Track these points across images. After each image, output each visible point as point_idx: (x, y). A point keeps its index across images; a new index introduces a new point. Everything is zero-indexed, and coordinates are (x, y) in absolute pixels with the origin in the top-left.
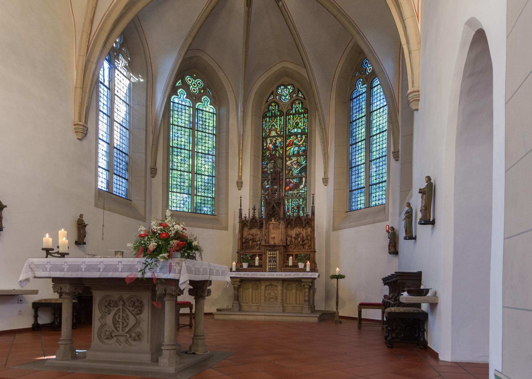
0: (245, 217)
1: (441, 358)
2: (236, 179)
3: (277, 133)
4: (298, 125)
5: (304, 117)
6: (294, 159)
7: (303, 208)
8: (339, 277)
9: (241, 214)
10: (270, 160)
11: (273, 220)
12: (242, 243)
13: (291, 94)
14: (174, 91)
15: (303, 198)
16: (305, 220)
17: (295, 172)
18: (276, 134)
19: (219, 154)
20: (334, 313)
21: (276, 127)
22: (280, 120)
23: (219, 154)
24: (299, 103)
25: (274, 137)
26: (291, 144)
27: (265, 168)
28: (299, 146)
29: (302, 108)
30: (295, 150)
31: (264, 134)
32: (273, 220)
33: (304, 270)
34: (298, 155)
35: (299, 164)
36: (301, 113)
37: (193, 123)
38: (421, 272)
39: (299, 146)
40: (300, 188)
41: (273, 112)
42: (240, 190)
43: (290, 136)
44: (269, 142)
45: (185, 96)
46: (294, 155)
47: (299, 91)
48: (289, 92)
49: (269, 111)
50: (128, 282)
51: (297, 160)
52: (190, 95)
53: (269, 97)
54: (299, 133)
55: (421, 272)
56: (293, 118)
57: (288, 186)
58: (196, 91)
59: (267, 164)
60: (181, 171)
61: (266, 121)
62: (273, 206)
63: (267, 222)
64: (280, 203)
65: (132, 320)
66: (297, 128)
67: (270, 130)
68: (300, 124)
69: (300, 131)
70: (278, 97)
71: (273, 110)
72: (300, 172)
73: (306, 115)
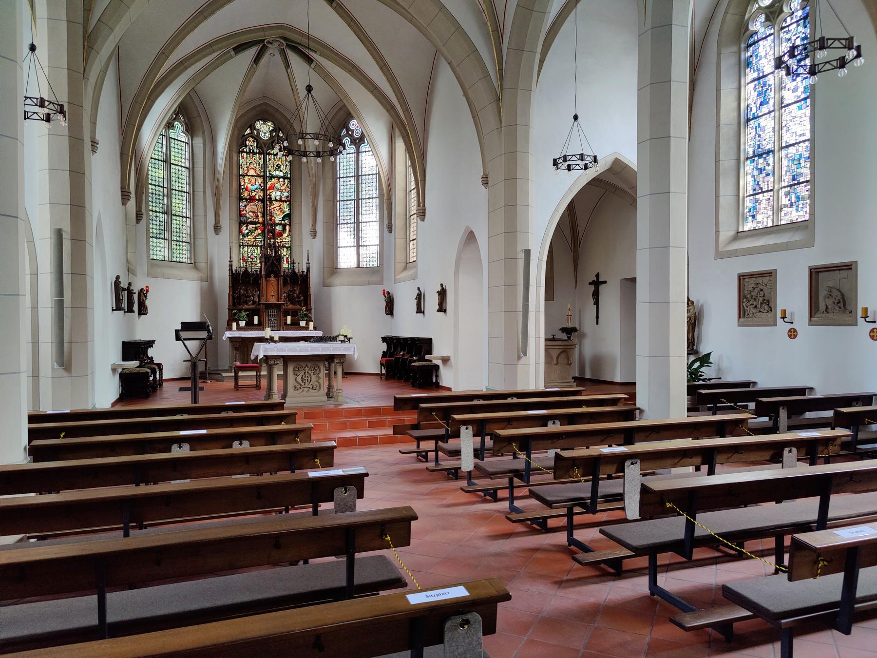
6: (276, 204)
15: (287, 248)
17: (278, 218)
19: (193, 191)
26: (272, 187)
28: (281, 191)
33: (306, 328)
34: (281, 200)
38: (431, 339)
44: (247, 181)
46: (276, 200)
47: (280, 130)
50: (860, 403)
54: (281, 177)
55: (431, 339)
59: (245, 206)
60: (156, 212)
61: (243, 157)
64: (279, 258)
65: (314, 378)
69: (281, 174)
72: (283, 219)
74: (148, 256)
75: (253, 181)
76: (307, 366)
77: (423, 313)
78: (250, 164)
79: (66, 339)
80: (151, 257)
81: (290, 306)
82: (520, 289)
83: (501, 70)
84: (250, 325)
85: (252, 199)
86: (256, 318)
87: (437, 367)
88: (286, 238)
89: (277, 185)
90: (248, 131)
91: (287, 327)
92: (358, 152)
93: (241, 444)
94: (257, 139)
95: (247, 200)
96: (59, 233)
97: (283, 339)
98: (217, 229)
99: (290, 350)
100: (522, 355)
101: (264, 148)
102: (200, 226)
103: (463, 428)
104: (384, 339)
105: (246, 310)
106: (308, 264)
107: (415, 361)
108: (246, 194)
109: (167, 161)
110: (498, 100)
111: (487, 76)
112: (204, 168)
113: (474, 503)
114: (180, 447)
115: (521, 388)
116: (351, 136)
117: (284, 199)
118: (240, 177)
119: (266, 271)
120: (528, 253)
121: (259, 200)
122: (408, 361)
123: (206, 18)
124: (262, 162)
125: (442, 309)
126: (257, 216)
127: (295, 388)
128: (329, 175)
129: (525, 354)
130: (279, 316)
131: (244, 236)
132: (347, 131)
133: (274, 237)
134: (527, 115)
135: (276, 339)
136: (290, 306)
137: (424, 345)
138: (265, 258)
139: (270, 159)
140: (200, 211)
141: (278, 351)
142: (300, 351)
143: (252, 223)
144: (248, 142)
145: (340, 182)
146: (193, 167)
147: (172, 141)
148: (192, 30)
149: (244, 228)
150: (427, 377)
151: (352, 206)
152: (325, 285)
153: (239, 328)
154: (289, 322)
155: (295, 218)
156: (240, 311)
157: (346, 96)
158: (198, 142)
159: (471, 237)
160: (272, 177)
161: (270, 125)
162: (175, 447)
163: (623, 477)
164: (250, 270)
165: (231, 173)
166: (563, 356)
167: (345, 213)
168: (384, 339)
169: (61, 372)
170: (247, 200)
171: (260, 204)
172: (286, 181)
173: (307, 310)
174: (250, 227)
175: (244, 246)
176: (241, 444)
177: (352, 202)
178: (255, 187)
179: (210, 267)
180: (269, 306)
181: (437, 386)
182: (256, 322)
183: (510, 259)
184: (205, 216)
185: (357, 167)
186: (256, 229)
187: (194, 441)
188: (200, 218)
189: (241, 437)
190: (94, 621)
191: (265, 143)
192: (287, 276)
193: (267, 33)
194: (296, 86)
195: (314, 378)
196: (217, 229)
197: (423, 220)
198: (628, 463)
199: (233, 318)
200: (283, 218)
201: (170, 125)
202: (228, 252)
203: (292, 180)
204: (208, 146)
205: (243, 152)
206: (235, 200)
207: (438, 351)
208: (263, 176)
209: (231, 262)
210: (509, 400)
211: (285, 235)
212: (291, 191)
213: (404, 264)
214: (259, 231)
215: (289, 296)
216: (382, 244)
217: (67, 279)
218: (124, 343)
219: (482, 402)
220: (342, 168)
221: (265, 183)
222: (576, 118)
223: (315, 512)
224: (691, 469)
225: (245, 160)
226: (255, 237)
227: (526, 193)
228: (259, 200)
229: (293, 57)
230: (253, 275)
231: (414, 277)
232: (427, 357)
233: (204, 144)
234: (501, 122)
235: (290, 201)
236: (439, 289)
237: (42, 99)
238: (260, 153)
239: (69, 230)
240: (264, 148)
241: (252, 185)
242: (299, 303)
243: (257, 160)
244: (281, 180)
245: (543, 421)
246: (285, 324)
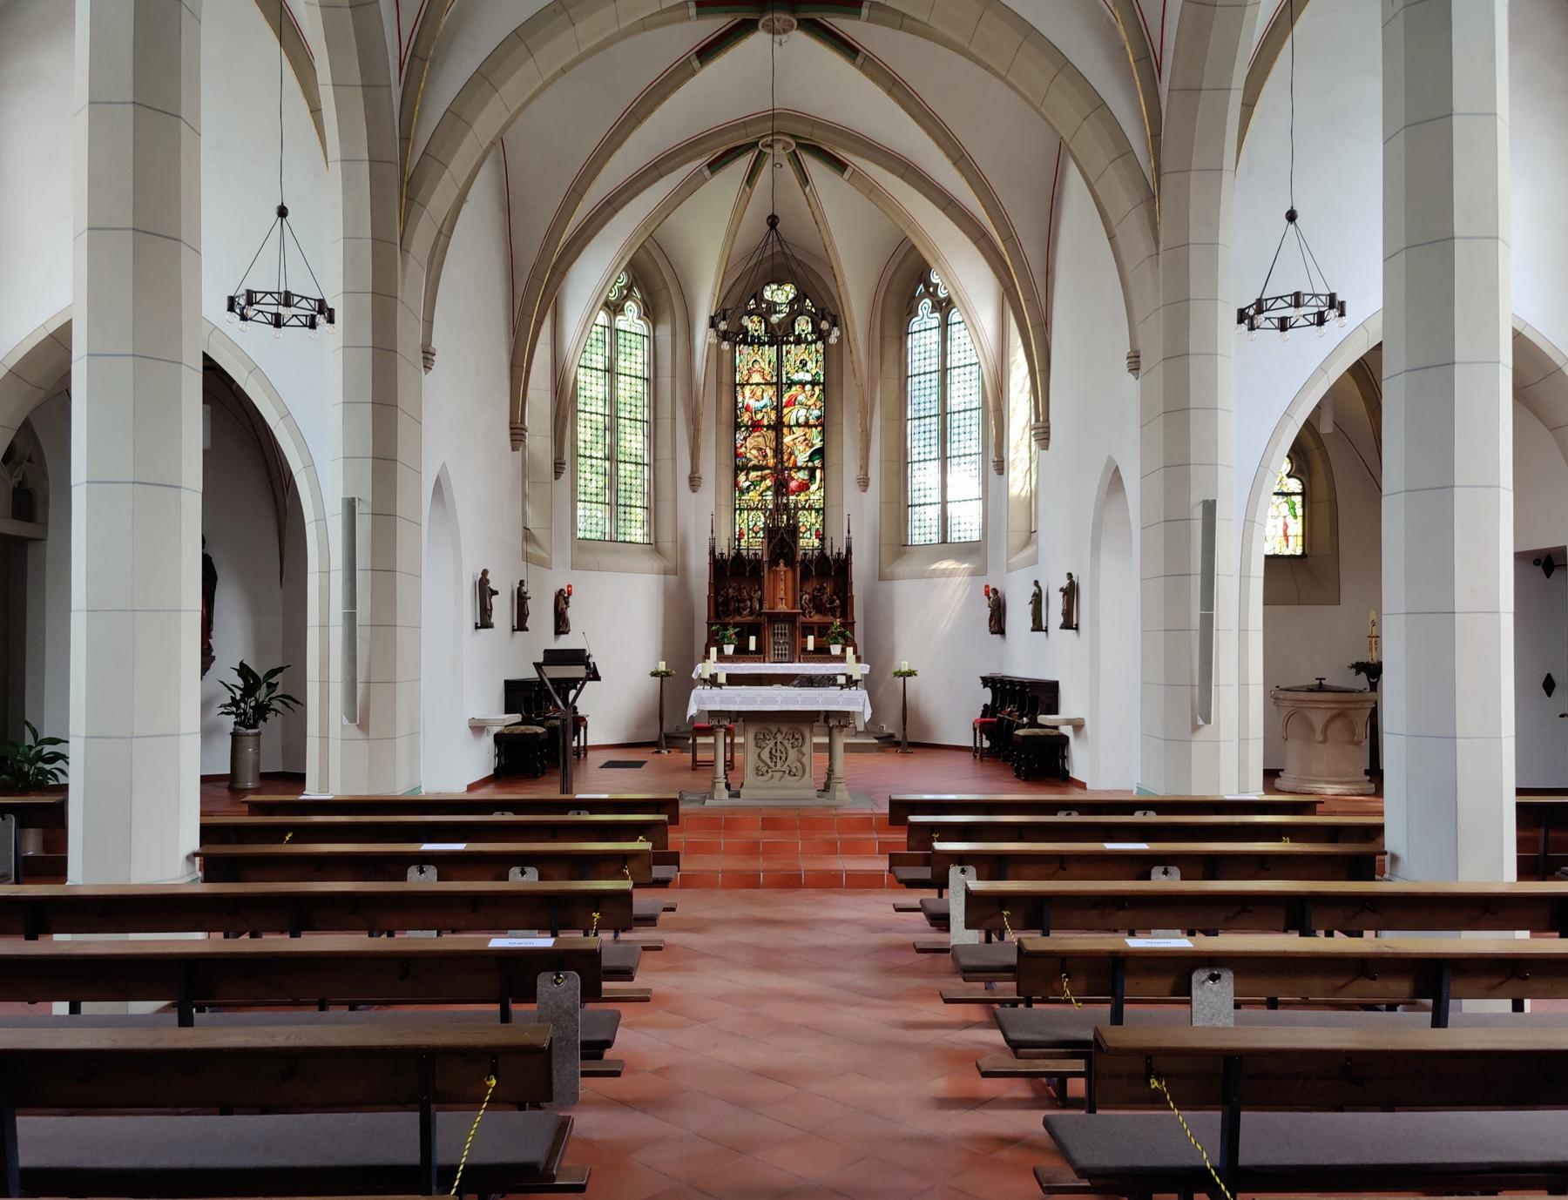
1: (1080, 763)
2: (687, 471)
6: (799, 432)
8: (911, 673)
9: (712, 552)
12: (717, 604)
15: (817, 511)
17: (802, 458)
20: (499, 738)
26: (792, 403)
28: (808, 408)
33: (842, 658)
34: (807, 425)
43: (790, 387)
46: (798, 425)
47: (806, 297)
63: (770, 567)
64: (793, 531)
65: (792, 753)
69: (808, 377)
72: (811, 458)
74: (574, 534)
75: (759, 393)
76: (779, 731)
77: (1077, 628)
78: (755, 362)
79: (361, 676)
80: (580, 535)
81: (816, 618)
82: (1196, 583)
83: (1156, 135)
84: (742, 652)
85: (756, 426)
86: (753, 639)
87: (1064, 740)
88: (815, 494)
89: (801, 398)
91: (806, 656)
92: (944, 325)
93: (523, 873)
95: (747, 427)
96: (350, 505)
97: (733, 680)
98: (694, 482)
99: (744, 701)
100: (1201, 722)
103: (954, 871)
104: (987, 681)
105: (735, 625)
107: (1024, 726)
108: (746, 417)
109: (611, 371)
110: (1151, 198)
111: (1125, 151)
112: (674, 377)
113: (968, 1025)
114: (422, 872)
115: (1199, 790)
116: (933, 296)
117: (812, 422)
119: (771, 554)
120: (1210, 508)
121: (769, 427)
122: (1021, 725)
123: (640, 122)
125: (1069, 624)
126: (765, 456)
127: (758, 772)
128: (891, 369)
129: (1207, 720)
130: (792, 635)
131: (742, 492)
132: (927, 287)
133: (787, 495)
134: (1212, 222)
135: (722, 679)
136: (816, 618)
137: (1044, 695)
138: (771, 532)
140: (665, 453)
141: (722, 702)
142: (762, 703)
143: (755, 468)
145: (913, 384)
146: (656, 377)
147: (621, 334)
148: (620, 144)
149: (742, 477)
150: (1045, 759)
151: (934, 427)
152: (882, 577)
153: (722, 658)
154: (811, 646)
156: (725, 627)
157: (911, 223)
158: (664, 331)
159: (1115, 481)
160: (791, 384)
161: (789, 291)
162: (413, 872)
163: (1189, 1003)
164: (744, 553)
165: (719, 383)
166: (1338, 724)
167: (921, 441)
168: (987, 681)
169: (353, 731)
170: (747, 427)
171: (771, 434)
172: (817, 389)
173: (842, 625)
174: (753, 474)
176: (523, 873)
177: (934, 420)
178: (762, 403)
179: (682, 547)
180: (775, 618)
181: (1062, 777)
182: (752, 646)
183: (1174, 520)
184: (674, 459)
185: (944, 354)
186: (763, 478)
187: (447, 865)
188: (665, 464)
189: (524, 860)
190: (413, 1157)
192: (811, 561)
193: (816, 131)
194: (822, 214)
195: (792, 753)
196: (694, 482)
197: (1046, 448)
198: (1199, 976)
199: (715, 640)
201: (614, 308)
202: (721, 520)
203: (827, 387)
204: (681, 339)
206: (726, 430)
207: (1071, 705)
210: (1138, 817)
211: (814, 487)
213: (1024, 535)
214: (768, 482)
215: (813, 599)
216: (985, 498)
217: (363, 579)
218: (507, 683)
219: (1075, 818)
220: (916, 357)
221: (780, 395)
222: (1291, 216)
223: (505, 1017)
224: (1505, 1005)
225: (745, 355)
226: (760, 493)
227: (1212, 384)
228: (769, 427)
229: (813, 165)
230: (750, 561)
231: (1034, 561)
232: (1043, 719)
233: (674, 335)
234: (1157, 242)
235: (822, 425)
236: (1065, 583)
237: (287, 293)
239: (369, 498)
241: (756, 400)
242: (833, 612)
244: (808, 387)
245: (1141, 866)
246: (804, 650)
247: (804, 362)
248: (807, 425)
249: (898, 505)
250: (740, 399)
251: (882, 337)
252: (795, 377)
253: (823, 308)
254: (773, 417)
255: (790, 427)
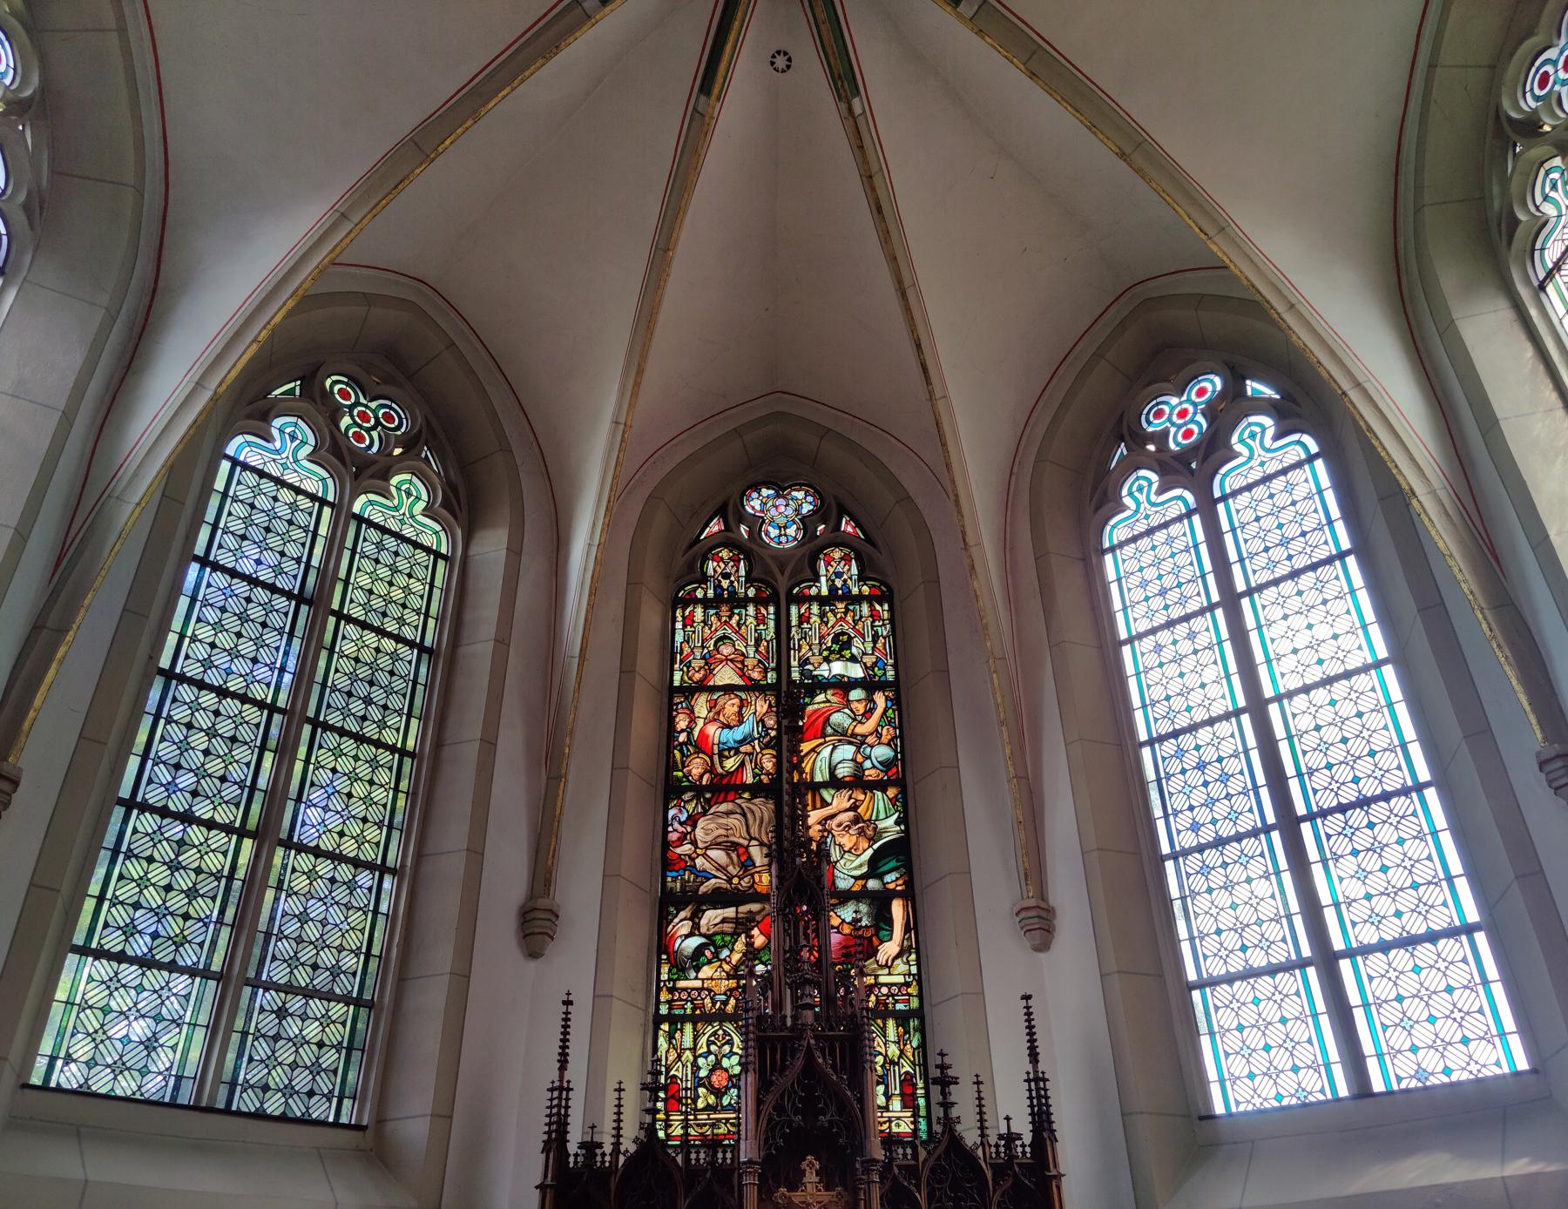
0: (590, 1147)
3: (742, 675)
4: (848, 645)
5: (874, 615)
7: (907, 1081)
9: (556, 1141)
10: (710, 803)
11: (811, 1177)
13: (806, 523)
14: (248, 407)
15: (902, 1019)
16: (1000, 1170)
18: (738, 681)
19: (438, 744)
21: (740, 646)
22: (761, 620)
23: (438, 744)
24: (846, 559)
25: (729, 689)
26: (821, 728)
27: (681, 841)
28: (859, 742)
29: (862, 578)
30: (838, 756)
31: (677, 676)
32: (811, 1177)
34: (858, 782)
35: (863, 826)
36: (859, 599)
37: (327, 576)
39: (859, 742)
40: (882, 957)
41: (725, 583)
42: (534, 954)
45: (308, 449)
46: (835, 783)
47: (842, 511)
48: (797, 511)
49: (704, 579)
51: (854, 808)
52: (333, 451)
53: (707, 525)
54: (854, 684)
56: (822, 615)
57: (880, 877)
58: (372, 443)
59: (692, 821)
61: (688, 621)
62: (810, 1067)
63: (765, 1191)
66: (841, 658)
67: (709, 662)
68: (857, 642)
69: (856, 672)
70: (743, 529)
71: (726, 576)
72: (875, 868)
73: (883, 610)
78: (725, 645)
90: (715, 526)
94: (750, 551)
95: (699, 791)
101: (778, 582)
102: (443, 906)
106: (1037, 1084)
108: (696, 767)
112: (502, 642)
117: (871, 774)
118: (673, 697)
119: (770, 1132)
121: (756, 790)
124: (771, 633)
126: (747, 865)
131: (681, 967)
138: (769, 1048)
139: (803, 619)
140: (453, 834)
143: (719, 898)
144: (711, 565)
155: (934, 858)
172: (880, 699)
174: (711, 917)
175: (676, 1021)
178: (739, 733)
186: (743, 925)
188: (449, 865)
191: (782, 559)
192: (912, 1171)
196: (536, 926)
200: (873, 862)
205: (691, 600)
206: (639, 794)
208: (774, 688)
209: (561, 1090)
211: (889, 949)
212: (903, 739)
225: (696, 630)
228: (756, 790)
230: (692, 1172)
233: (515, 552)
235: (900, 783)
238: (759, 601)
240: (778, 582)
243: (752, 627)
247: (845, 648)
248: (858, 782)
249: (1154, 1001)
250: (682, 723)
251: (1041, 558)
252: (823, 671)
253: (880, 528)
254: (768, 765)
255: (816, 787)
